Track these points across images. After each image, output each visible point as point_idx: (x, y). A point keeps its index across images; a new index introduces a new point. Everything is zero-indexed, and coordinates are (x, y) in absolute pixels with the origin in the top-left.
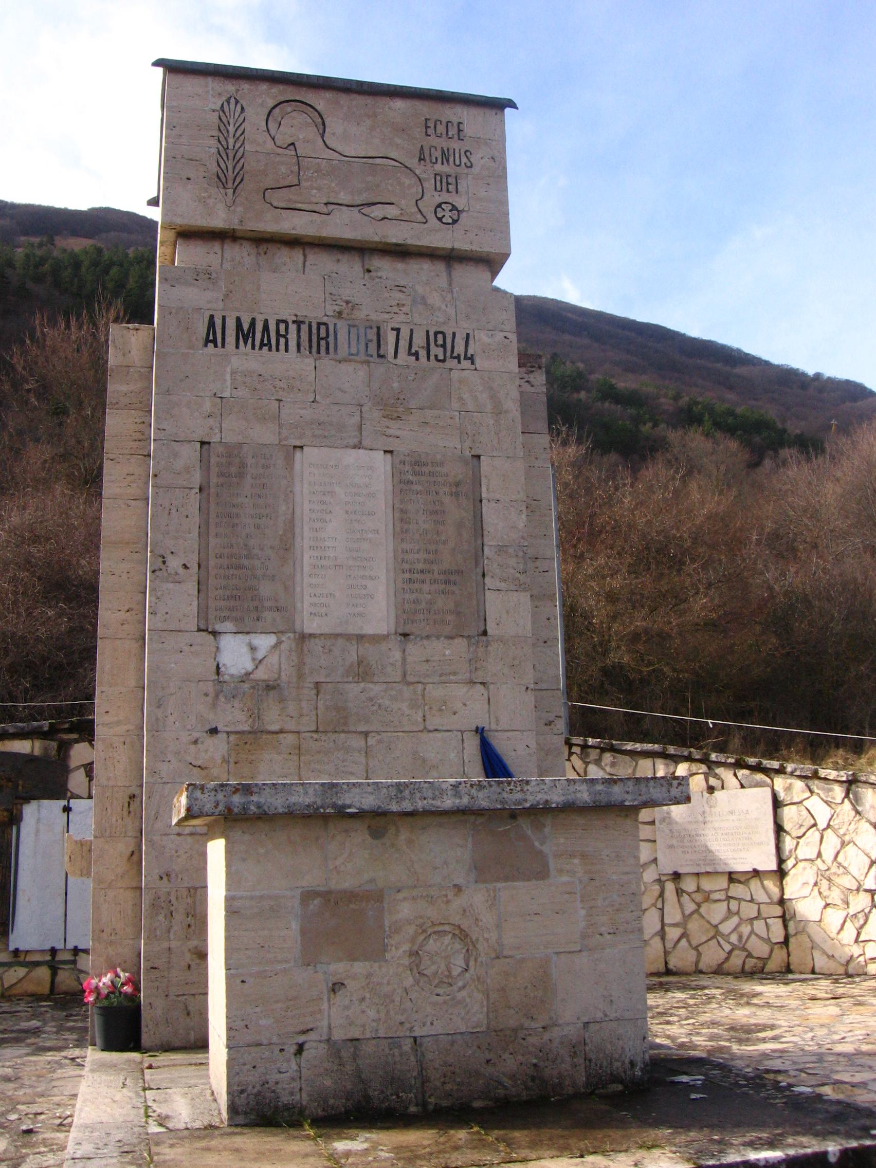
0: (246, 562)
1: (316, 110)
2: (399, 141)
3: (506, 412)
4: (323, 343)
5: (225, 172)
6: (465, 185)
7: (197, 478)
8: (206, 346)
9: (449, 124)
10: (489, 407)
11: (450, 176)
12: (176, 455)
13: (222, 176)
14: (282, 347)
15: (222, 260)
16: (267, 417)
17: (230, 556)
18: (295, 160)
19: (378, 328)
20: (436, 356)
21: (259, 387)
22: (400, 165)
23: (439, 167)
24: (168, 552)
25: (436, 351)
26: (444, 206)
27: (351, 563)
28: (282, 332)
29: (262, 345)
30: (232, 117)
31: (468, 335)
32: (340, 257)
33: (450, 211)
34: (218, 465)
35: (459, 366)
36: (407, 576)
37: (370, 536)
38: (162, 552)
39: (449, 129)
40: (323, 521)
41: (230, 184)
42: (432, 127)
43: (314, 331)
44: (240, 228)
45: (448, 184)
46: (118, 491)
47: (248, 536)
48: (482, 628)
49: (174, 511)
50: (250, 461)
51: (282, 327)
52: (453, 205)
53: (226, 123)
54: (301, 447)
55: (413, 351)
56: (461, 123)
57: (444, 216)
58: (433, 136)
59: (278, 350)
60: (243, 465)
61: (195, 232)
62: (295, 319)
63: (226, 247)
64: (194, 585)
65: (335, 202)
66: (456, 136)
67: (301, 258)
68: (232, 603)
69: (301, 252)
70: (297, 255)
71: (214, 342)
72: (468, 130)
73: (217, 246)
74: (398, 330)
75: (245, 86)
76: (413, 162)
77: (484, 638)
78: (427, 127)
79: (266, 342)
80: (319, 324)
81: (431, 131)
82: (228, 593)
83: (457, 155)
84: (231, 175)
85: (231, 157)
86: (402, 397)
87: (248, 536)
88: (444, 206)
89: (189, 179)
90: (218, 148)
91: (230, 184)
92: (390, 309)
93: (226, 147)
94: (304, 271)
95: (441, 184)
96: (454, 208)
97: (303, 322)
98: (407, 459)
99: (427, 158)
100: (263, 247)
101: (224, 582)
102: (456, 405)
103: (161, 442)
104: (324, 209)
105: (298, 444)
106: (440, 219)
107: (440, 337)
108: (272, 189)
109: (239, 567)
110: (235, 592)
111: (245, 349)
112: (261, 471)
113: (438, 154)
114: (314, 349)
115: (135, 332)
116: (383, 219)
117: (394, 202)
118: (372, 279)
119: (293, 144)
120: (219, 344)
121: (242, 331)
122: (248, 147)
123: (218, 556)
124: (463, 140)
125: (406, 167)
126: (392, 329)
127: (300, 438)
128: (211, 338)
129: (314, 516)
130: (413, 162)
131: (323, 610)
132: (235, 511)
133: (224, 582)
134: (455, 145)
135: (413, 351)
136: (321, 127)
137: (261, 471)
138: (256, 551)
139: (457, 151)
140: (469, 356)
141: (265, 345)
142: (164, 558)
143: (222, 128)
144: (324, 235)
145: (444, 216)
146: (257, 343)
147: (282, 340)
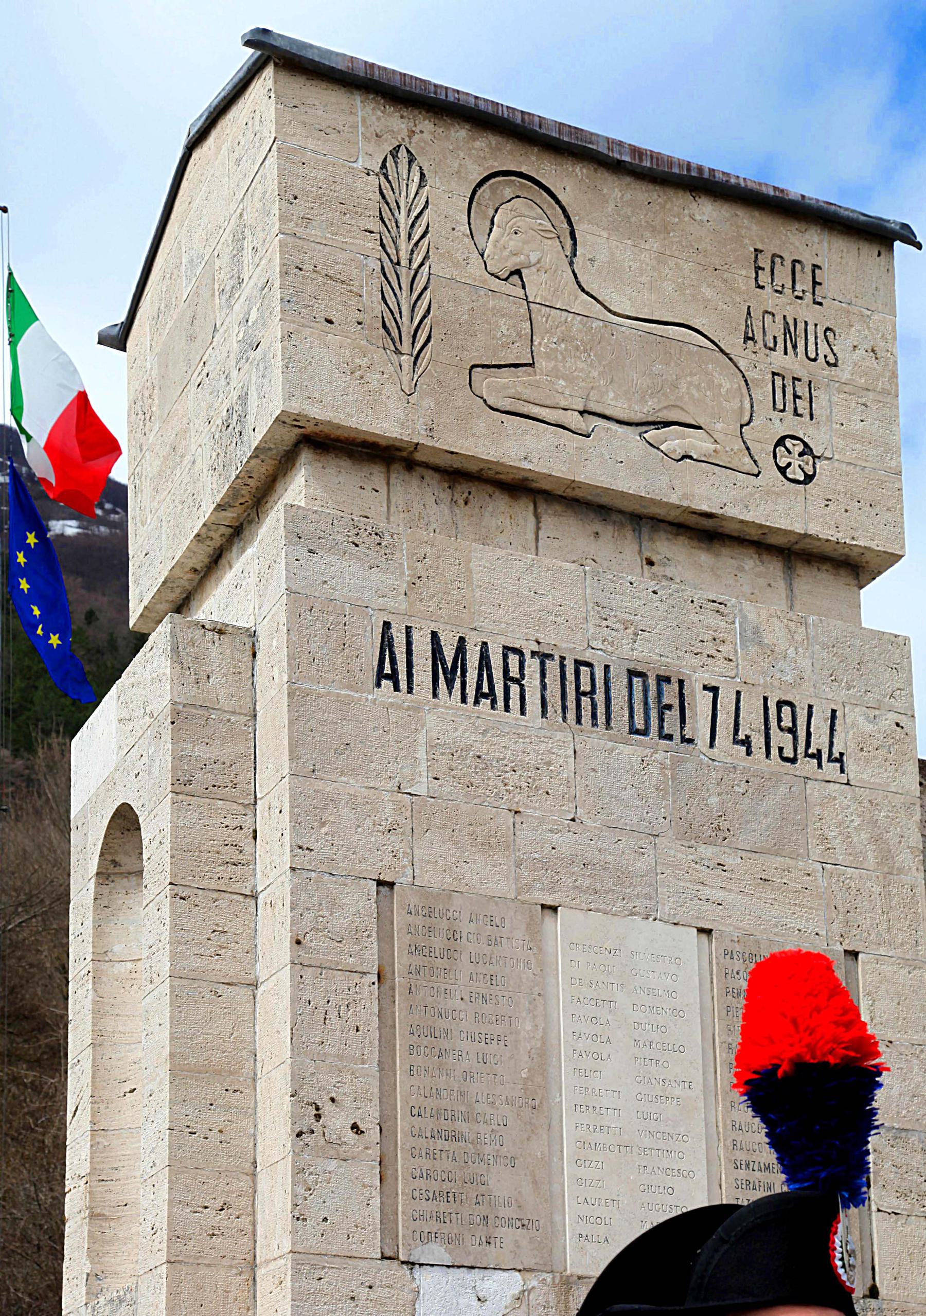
0: (462, 1127)
1: (558, 202)
2: (708, 293)
3: (900, 871)
4: (585, 701)
5: (397, 316)
6: (825, 403)
7: (371, 959)
8: (378, 685)
9: (798, 266)
10: (871, 860)
11: (799, 380)
12: (334, 905)
13: (390, 324)
14: (514, 703)
15: (389, 508)
16: (493, 841)
17: (438, 1114)
18: (523, 310)
19: (681, 683)
20: (781, 749)
21: (476, 780)
22: (715, 348)
23: (778, 360)
24: (326, 1098)
25: (781, 739)
26: (789, 443)
27: (647, 1142)
28: (514, 672)
29: (480, 695)
30: (404, 194)
31: (834, 712)
32: (598, 526)
33: (801, 455)
34: (409, 930)
35: (820, 774)
36: (742, 1174)
37: (677, 1092)
38: (313, 1097)
39: (797, 278)
40: (597, 1056)
41: (406, 347)
42: (768, 269)
43: (570, 677)
44: (429, 443)
45: (796, 396)
46: (199, 963)
47: (467, 1075)
48: (869, 1283)
49: (333, 1015)
50: (466, 927)
51: (513, 660)
52: (806, 445)
53: (393, 205)
54: (554, 909)
55: (741, 736)
56: (819, 267)
57: (789, 464)
58: (768, 289)
59: (507, 708)
60: (454, 936)
61: (338, 440)
62: (535, 648)
63: (393, 476)
64: (373, 1168)
65: (598, 411)
66: (809, 296)
67: (532, 519)
68: (443, 1207)
69: (531, 508)
70: (524, 512)
71: (393, 677)
72: (831, 285)
73: (377, 476)
74: (715, 690)
75: (426, 126)
76: (733, 343)
77: (873, 1303)
78: (758, 268)
79: (485, 689)
80: (578, 663)
81: (764, 278)
82: (435, 1186)
83: (811, 338)
84: (407, 329)
85: (405, 284)
86: (724, 825)
87: (467, 1075)
88: (789, 443)
89: (330, 322)
90: (380, 260)
91: (406, 347)
92: (699, 646)
93: (395, 261)
94: (537, 548)
95: (784, 396)
96: (807, 450)
97: (550, 656)
98: (738, 948)
99: (759, 336)
100: (462, 488)
101: (426, 1164)
102: (816, 852)
103: (305, 874)
104: (573, 420)
105: (549, 902)
106: (783, 470)
107: (786, 710)
108: (483, 366)
109: (454, 1137)
110: (446, 1186)
111: (449, 700)
112: (487, 950)
113: (777, 329)
114: (571, 715)
115: (217, 636)
116: (684, 457)
117: (700, 422)
118: (654, 577)
119: (518, 272)
120: (403, 685)
121: (444, 663)
122: (436, 266)
123: (415, 1111)
124: (820, 304)
125: (722, 351)
126: (705, 688)
127: (552, 891)
128: (387, 670)
129: (580, 1046)
130: (733, 343)
131: (602, 1230)
132: (442, 1023)
133: (426, 1164)
134: (805, 312)
135: (741, 736)
136: (568, 243)
137: (487, 950)
138: (479, 1108)
139: (811, 328)
140: (836, 754)
141: (485, 696)
142: (317, 1109)
143: (386, 215)
144: (581, 478)
145: (789, 464)
146: (471, 691)
147: (514, 689)
